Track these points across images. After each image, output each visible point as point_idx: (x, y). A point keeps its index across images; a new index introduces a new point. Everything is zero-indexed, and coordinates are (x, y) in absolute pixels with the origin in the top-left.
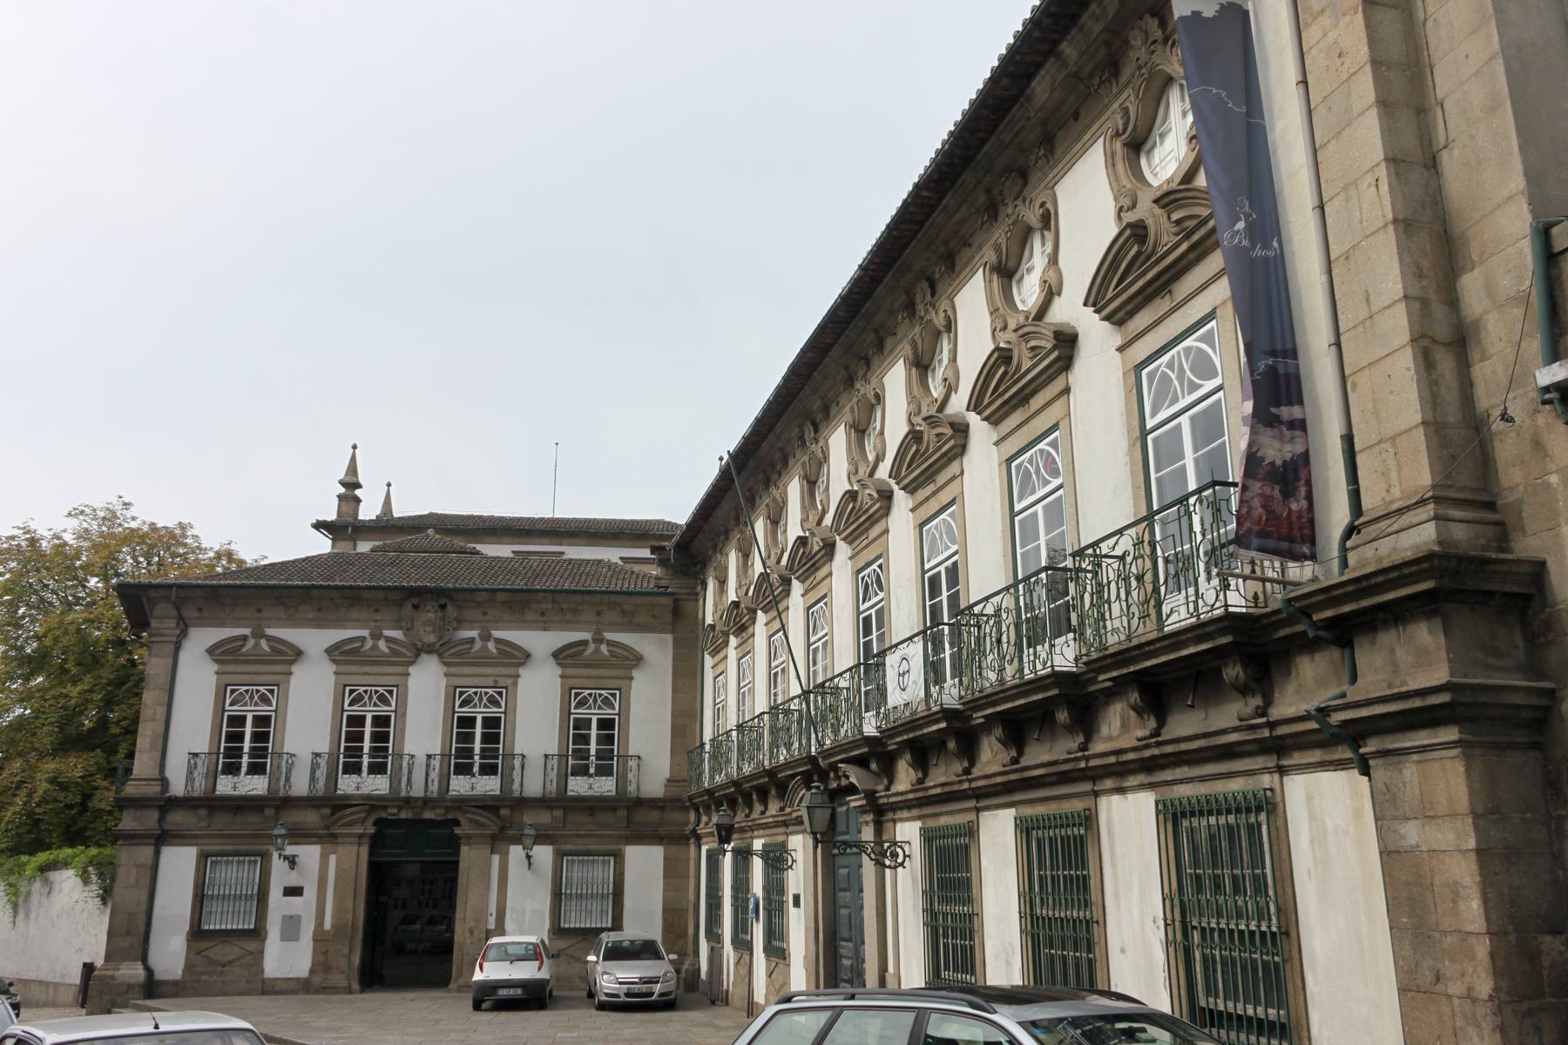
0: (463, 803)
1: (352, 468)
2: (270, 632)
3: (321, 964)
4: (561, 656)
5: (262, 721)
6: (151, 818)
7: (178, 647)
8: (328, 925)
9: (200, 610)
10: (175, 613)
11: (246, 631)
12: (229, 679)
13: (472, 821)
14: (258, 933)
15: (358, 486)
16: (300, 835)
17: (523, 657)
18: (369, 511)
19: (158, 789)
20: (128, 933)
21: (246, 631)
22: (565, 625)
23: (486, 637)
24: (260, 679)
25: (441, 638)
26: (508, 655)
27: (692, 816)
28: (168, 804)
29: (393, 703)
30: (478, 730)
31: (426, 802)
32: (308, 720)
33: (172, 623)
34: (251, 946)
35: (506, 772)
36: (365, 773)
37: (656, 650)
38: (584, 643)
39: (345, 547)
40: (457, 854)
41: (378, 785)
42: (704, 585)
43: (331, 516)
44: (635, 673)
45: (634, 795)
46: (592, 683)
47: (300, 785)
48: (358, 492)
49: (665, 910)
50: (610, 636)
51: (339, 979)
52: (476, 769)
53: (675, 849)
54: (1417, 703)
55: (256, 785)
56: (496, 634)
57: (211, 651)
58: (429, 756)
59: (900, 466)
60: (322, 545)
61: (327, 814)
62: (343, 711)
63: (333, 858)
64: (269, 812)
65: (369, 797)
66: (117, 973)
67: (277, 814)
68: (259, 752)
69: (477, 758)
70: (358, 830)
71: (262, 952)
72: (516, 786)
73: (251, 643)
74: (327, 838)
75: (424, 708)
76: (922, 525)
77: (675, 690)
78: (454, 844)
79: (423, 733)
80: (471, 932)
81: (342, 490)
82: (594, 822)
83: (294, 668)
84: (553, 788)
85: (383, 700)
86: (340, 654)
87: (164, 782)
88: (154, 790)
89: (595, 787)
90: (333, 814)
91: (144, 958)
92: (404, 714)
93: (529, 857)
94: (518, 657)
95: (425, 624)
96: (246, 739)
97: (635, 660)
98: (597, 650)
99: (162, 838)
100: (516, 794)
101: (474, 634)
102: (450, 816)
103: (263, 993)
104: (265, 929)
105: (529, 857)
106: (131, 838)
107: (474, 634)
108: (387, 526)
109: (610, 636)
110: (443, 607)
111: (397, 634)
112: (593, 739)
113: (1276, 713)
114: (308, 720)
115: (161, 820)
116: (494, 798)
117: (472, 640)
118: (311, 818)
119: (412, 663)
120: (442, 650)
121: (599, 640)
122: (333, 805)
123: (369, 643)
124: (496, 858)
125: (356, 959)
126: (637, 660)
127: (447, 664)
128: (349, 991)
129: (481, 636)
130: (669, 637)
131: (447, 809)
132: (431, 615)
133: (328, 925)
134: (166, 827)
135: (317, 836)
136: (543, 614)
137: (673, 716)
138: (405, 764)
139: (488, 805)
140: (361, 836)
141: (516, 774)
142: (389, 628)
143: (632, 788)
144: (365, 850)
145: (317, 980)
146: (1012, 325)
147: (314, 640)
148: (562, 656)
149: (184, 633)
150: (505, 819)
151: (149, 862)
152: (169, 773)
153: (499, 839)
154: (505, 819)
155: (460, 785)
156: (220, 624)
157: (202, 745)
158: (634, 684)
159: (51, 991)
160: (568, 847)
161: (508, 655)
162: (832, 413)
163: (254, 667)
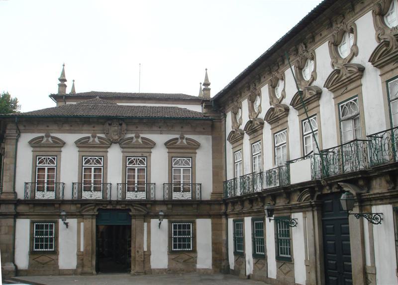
0: (132, 203)
1: (63, 74)
2: (52, 135)
5: (97, 170)
6: (11, 209)
7: (17, 140)
8: (82, 249)
9: (25, 126)
10: (15, 127)
11: (43, 135)
12: (37, 153)
13: (136, 209)
15: (65, 80)
16: (71, 215)
18: (68, 91)
19: (14, 196)
21: (43, 135)
22: (168, 132)
23: (137, 137)
25: (120, 137)
26: (146, 144)
27: (223, 207)
28: (17, 202)
29: (102, 163)
31: (118, 202)
32: (69, 168)
33: (14, 132)
34: (53, 257)
36: (45, 191)
37: (205, 142)
38: (177, 139)
39: (62, 104)
40: (131, 222)
42: (225, 116)
43: (56, 92)
44: (197, 151)
45: (153, 199)
47: (68, 196)
48: (65, 83)
50: (186, 136)
51: (86, 269)
52: (92, 189)
53: (216, 220)
55: (50, 195)
56: (142, 135)
57: (30, 142)
58: (73, 183)
59: (375, 56)
60: (52, 104)
61: (79, 208)
62: (36, 166)
63: (82, 224)
64: (57, 206)
65: (96, 200)
67: (60, 207)
69: (92, 184)
70: (91, 213)
71: (58, 259)
72: (108, 196)
73: (45, 139)
74: (79, 216)
76: (387, 81)
77: (213, 158)
78: (130, 218)
79: (114, 175)
81: (60, 82)
82: (182, 212)
83: (62, 149)
84: (167, 197)
85: (98, 162)
86: (80, 144)
87: (15, 193)
88: (11, 197)
89: (138, 196)
90: (81, 207)
91: (13, 261)
92: (107, 168)
94: (150, 145)
95: (115, 131)
96: (45, 175)
97: (197, 146)
98: (182, 142)
99: (17, 216)
100: (61, 199)
101: (133, 135)
102: (127, 208)
103: (59, 275)
104: (58, 250)
107: (133, 135)
108: (74, 96)
109: (186, 136)
110: (121, 125)
111: (102, 136)
114: (69, 168)
115: (15, 208)
116: (144, 200)
117: (132, 138)
118: (73, 208)
119: (109, 147)
120: (125, 144)
123: (91, 139)
124: (146, 224)
125: (94, 263)
127: (122, 148)
128: (92, 274)
129: (135, 136)
130: (210, 137)
131: (126, 205)
132: (116, 128)
133: (82, 249)
134: (18, 211)
135: (75, 215)
137: (213, 168)
138: (61, 187)
139: (141, 203)
140: (93, 215)
141: (108, 191)
142: (99, 133)
143: (152, 196)
144: (94, 221)
147: (70, 138)
148: (168, 145)
149: (19, 136)
151: (12, 225)
152: (17, 190)
153: (147, 217)
155: (130, 196)
156: (33, 132)
157: (29, 180)
158: (197, 155)
160: (173, 220)
161: (146, 144)
162: (317, 39)
163: (47, 151)
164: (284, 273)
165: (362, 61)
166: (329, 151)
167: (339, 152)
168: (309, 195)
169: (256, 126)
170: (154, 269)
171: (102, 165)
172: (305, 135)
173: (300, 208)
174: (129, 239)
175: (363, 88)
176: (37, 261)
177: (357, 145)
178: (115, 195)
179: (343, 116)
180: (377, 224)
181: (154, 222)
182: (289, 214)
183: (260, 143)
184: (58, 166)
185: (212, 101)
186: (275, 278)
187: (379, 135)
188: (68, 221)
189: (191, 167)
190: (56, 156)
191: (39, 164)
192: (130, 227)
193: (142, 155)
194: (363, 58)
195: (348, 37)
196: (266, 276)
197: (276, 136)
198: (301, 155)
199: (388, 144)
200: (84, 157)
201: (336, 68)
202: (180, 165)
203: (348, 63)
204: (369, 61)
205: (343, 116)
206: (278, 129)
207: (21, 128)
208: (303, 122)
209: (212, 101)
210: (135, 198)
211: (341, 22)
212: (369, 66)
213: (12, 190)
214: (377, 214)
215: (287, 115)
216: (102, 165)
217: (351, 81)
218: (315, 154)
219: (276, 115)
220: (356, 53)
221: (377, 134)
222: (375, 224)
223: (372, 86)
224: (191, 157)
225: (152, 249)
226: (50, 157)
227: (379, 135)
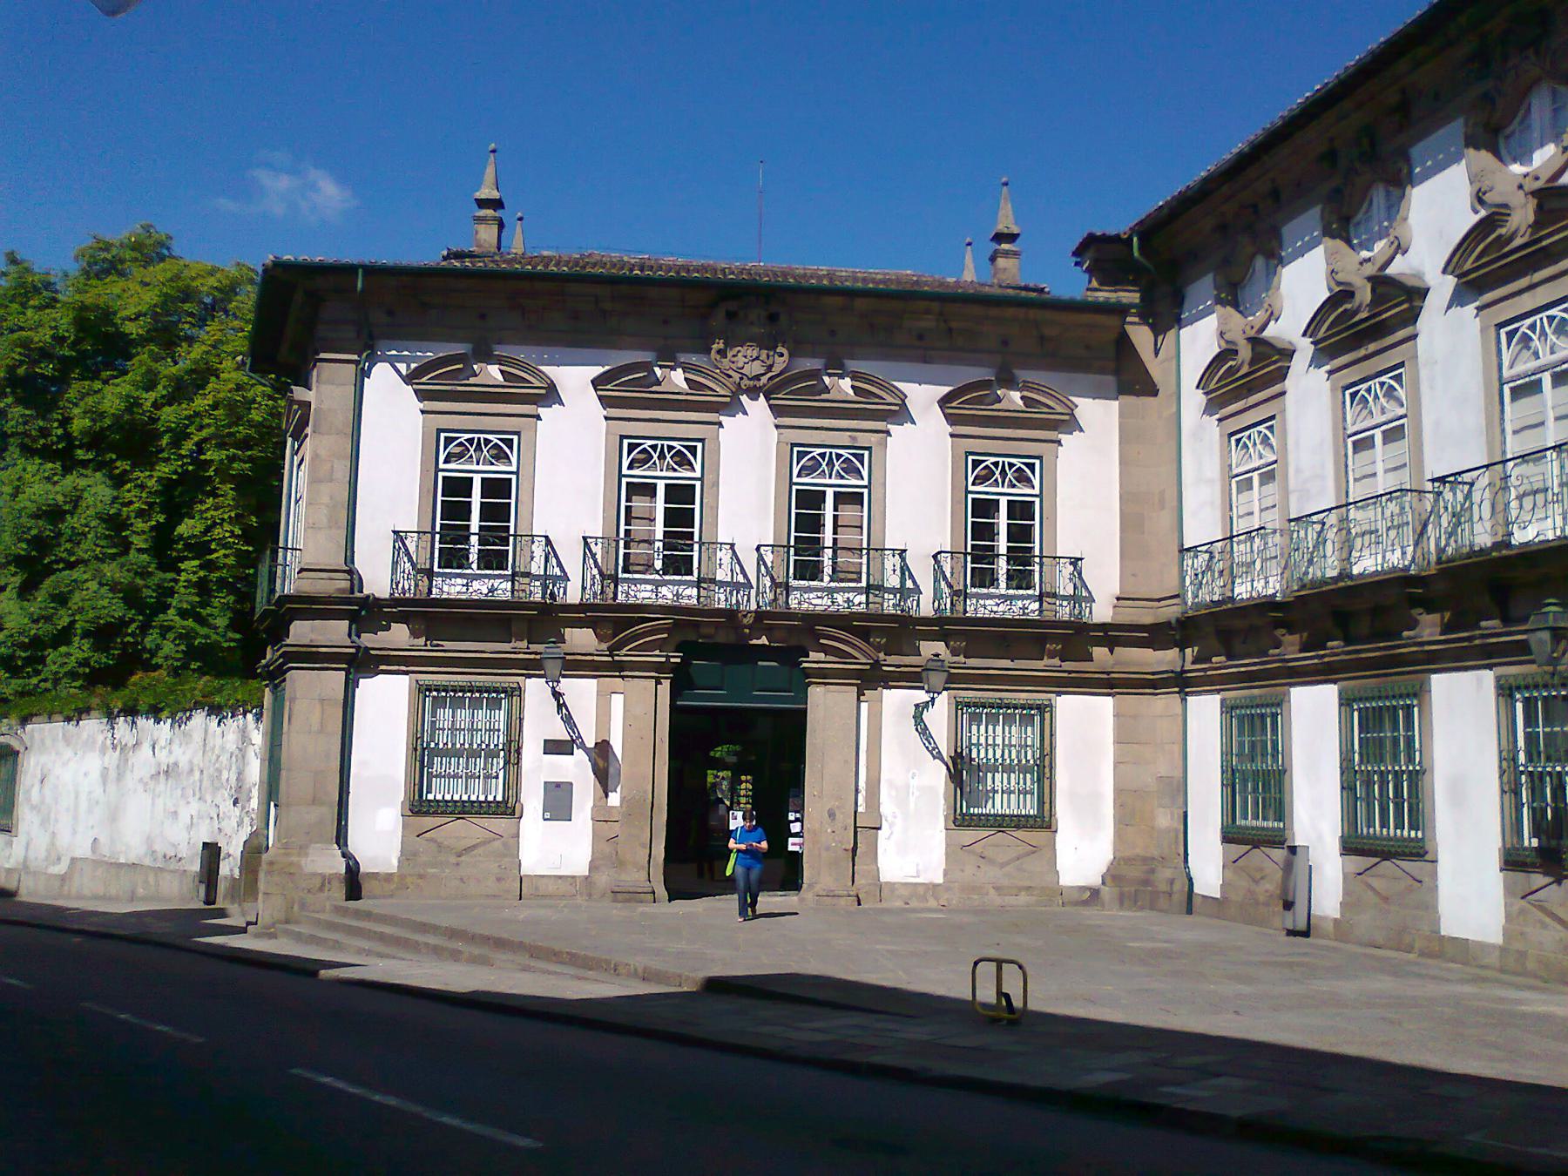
0: (812, 622)
3: (606, 851)
5: (1020, 510)
6: (334, 633)
9: (390, 313)
14: (508, 808)
19: (346, 585)
20: (315, 801)
28: (366, 612)
29: (698, 467)
30: (476, 499)
34: (499, 824)
55: (1026, 607)
62: (437, 470)
63: (617, 701)
68: (1020, 556)
70: (657, 657)
75: (746, 472)
78: (803, 680)
80: (832, 815)
91: (341, 837)
92: (716, 484)
93: (557, 695)
96: (474, 513)
99: (361, 664)
105: (557, 695)
106: (313, 657)
110: (773, 318)
112: (1001, 531)
120: (791, 397)
122: (613, 620)
136: (921, 337)
139: (858, 626)
140: (658, 667)
150: (883, 645)
157: (409, 519)
159: (151, 879)
170: (892, 885)
171: (698, 474)
174: (1506, 797)
176: (432, 840)
181: (896, 701)
184: (526, 469)
187: (1467, 477)
188: (566, 685)
189: (1040, 496)
190: (518, 433)
191: (446, 462)
192: (797, 720)
193: (854, 439)
198: (1224, 530)
200: (626, 442)
209: (1130, 240)
213: (339, 562)
216: (698, 474)
217: (1377, 330)
221: (1459, 473)
223: (1449, 338)
224: (1040, 458)
225: (887, 806)
226: (490, 437)
227: (1467, 477)
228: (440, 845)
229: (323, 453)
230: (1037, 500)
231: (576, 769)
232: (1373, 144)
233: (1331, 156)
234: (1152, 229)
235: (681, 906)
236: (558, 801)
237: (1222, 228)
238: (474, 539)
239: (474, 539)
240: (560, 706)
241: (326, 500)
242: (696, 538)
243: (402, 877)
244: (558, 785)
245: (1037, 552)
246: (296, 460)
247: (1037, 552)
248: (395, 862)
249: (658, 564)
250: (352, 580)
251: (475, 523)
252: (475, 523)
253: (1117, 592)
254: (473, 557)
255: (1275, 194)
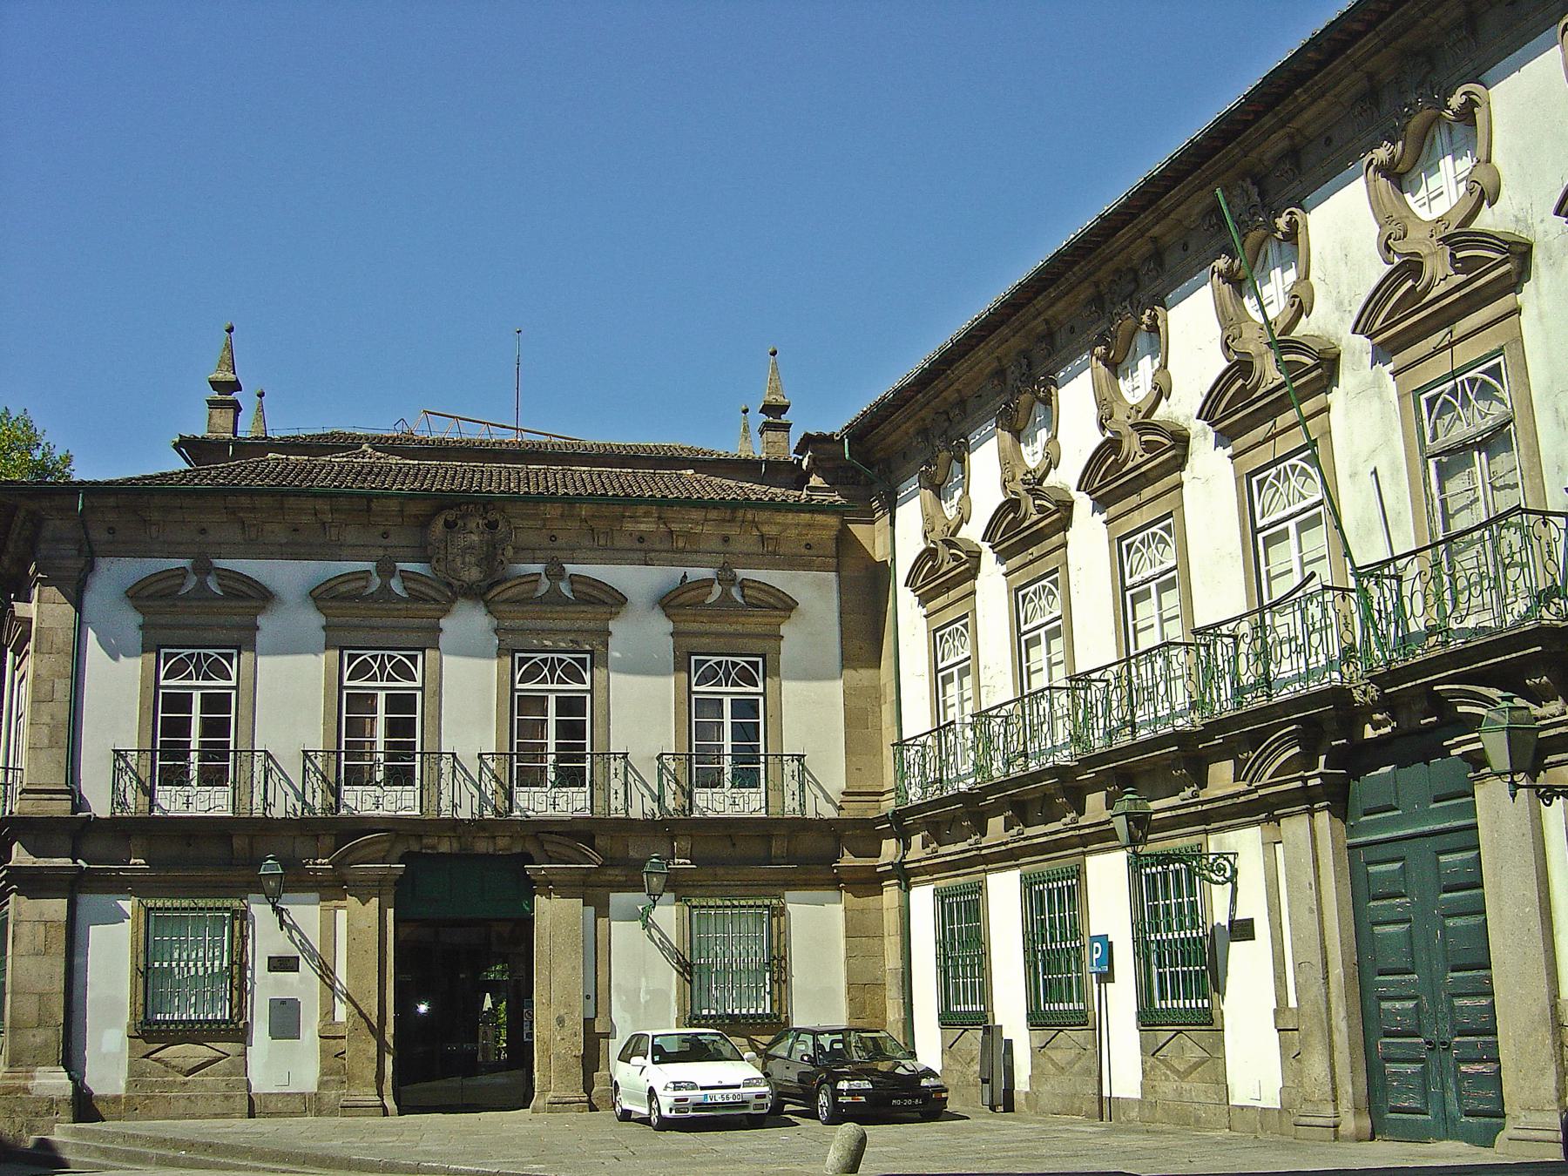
0: (542, 830)
3: (334, 1066)
4: (668, 603)
9: (111, 530)
14: (241, 1034)
17: (614, 601)
24: (209, 636)
29: (419, 676)
31: (478, 826)
35: (599, 779)
41: (402, 802)
46: (720, 644)
49: (850, 985)
54: (1229, 802)
61: (313, 853)
62: (341, 687)
63: (342, 915)
66: (30, 1084)
73: (191, 582)
78: (529, 888)
80: (561, 1021)
87: (79, 803)
89: (561, 802)
101: (537, 568)
107: (537, 568)
113: (1082, 821)
121: (727, 580)
126: (787, 606)
136: (641, 540)
139: (578, 832)
145: (331, 1094)
146: (1019, 477)
149: (91, 567)
150: (606, 858)
154: (606, 858)
155: (535, 802)
157: (130, 738)
164: (1177, 1072)
165: (1517, 220)
166: (1093, 676)
167: (1118, 677)
168: (1297, 749)
169: (1035, 518)
171: (418, 684)
172: (1263, 529)
173: (1261, 810)
175: (1526, 320)
177: (1168, 662)
178: (462, 801)
179: (1263, 516)
180: (1223, 883)
182: (1201, 838)
183: (1055, 582)
185: (842, 439)
186: (1136, 1094)
192: (526, 924)
194: (1183, 407)
195: (1446, 140)
196: (1091, 1090)
197: (941, 637)
199: (1425, 596)
201: (1108, 434)
202: (544, 681)
203: (1035, 483)
204: (1557, 213)
205: (1263, 516)
206: (1263, 455)
207: (99, 535)
208: (1124, 543)
209: (842, 439)
210: (550, 811)
211: (1420, 85)
212: (1356, 349)
214: (1220, 855)
215: (1180, 463)
217: (1039, 537)
218: (1325, 588)
219: (1130, 465)
220: (1489, 189)
221: (1218, 625)
222: (1217, 883)
228: (166, 1064)
229: (44, 673)
230: (761, 699)
231: (303, 984)
232: (1029, 365)
233: (1000, 373)
234: (864, 430)
235: (435, 1132)
236: (286, 1020)
237: (924, 432)
238: (194, 756)
239: (194, 756)
240: (282, 922)
241: (46, 719)
242: (418, 749)
243: (129, 1098)
244: (283, 1002)
245: (762, 751)
246: (18, 675)
247: (762, 751)
248: (123, 1084)
249: (379, 776)
250: (73, 800)
251: (195, 740)
252: (195, 740)
253: (844, 787)
254: (194, 774)
255: (962, 403)
